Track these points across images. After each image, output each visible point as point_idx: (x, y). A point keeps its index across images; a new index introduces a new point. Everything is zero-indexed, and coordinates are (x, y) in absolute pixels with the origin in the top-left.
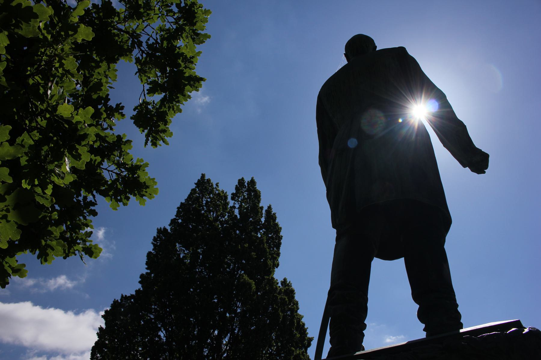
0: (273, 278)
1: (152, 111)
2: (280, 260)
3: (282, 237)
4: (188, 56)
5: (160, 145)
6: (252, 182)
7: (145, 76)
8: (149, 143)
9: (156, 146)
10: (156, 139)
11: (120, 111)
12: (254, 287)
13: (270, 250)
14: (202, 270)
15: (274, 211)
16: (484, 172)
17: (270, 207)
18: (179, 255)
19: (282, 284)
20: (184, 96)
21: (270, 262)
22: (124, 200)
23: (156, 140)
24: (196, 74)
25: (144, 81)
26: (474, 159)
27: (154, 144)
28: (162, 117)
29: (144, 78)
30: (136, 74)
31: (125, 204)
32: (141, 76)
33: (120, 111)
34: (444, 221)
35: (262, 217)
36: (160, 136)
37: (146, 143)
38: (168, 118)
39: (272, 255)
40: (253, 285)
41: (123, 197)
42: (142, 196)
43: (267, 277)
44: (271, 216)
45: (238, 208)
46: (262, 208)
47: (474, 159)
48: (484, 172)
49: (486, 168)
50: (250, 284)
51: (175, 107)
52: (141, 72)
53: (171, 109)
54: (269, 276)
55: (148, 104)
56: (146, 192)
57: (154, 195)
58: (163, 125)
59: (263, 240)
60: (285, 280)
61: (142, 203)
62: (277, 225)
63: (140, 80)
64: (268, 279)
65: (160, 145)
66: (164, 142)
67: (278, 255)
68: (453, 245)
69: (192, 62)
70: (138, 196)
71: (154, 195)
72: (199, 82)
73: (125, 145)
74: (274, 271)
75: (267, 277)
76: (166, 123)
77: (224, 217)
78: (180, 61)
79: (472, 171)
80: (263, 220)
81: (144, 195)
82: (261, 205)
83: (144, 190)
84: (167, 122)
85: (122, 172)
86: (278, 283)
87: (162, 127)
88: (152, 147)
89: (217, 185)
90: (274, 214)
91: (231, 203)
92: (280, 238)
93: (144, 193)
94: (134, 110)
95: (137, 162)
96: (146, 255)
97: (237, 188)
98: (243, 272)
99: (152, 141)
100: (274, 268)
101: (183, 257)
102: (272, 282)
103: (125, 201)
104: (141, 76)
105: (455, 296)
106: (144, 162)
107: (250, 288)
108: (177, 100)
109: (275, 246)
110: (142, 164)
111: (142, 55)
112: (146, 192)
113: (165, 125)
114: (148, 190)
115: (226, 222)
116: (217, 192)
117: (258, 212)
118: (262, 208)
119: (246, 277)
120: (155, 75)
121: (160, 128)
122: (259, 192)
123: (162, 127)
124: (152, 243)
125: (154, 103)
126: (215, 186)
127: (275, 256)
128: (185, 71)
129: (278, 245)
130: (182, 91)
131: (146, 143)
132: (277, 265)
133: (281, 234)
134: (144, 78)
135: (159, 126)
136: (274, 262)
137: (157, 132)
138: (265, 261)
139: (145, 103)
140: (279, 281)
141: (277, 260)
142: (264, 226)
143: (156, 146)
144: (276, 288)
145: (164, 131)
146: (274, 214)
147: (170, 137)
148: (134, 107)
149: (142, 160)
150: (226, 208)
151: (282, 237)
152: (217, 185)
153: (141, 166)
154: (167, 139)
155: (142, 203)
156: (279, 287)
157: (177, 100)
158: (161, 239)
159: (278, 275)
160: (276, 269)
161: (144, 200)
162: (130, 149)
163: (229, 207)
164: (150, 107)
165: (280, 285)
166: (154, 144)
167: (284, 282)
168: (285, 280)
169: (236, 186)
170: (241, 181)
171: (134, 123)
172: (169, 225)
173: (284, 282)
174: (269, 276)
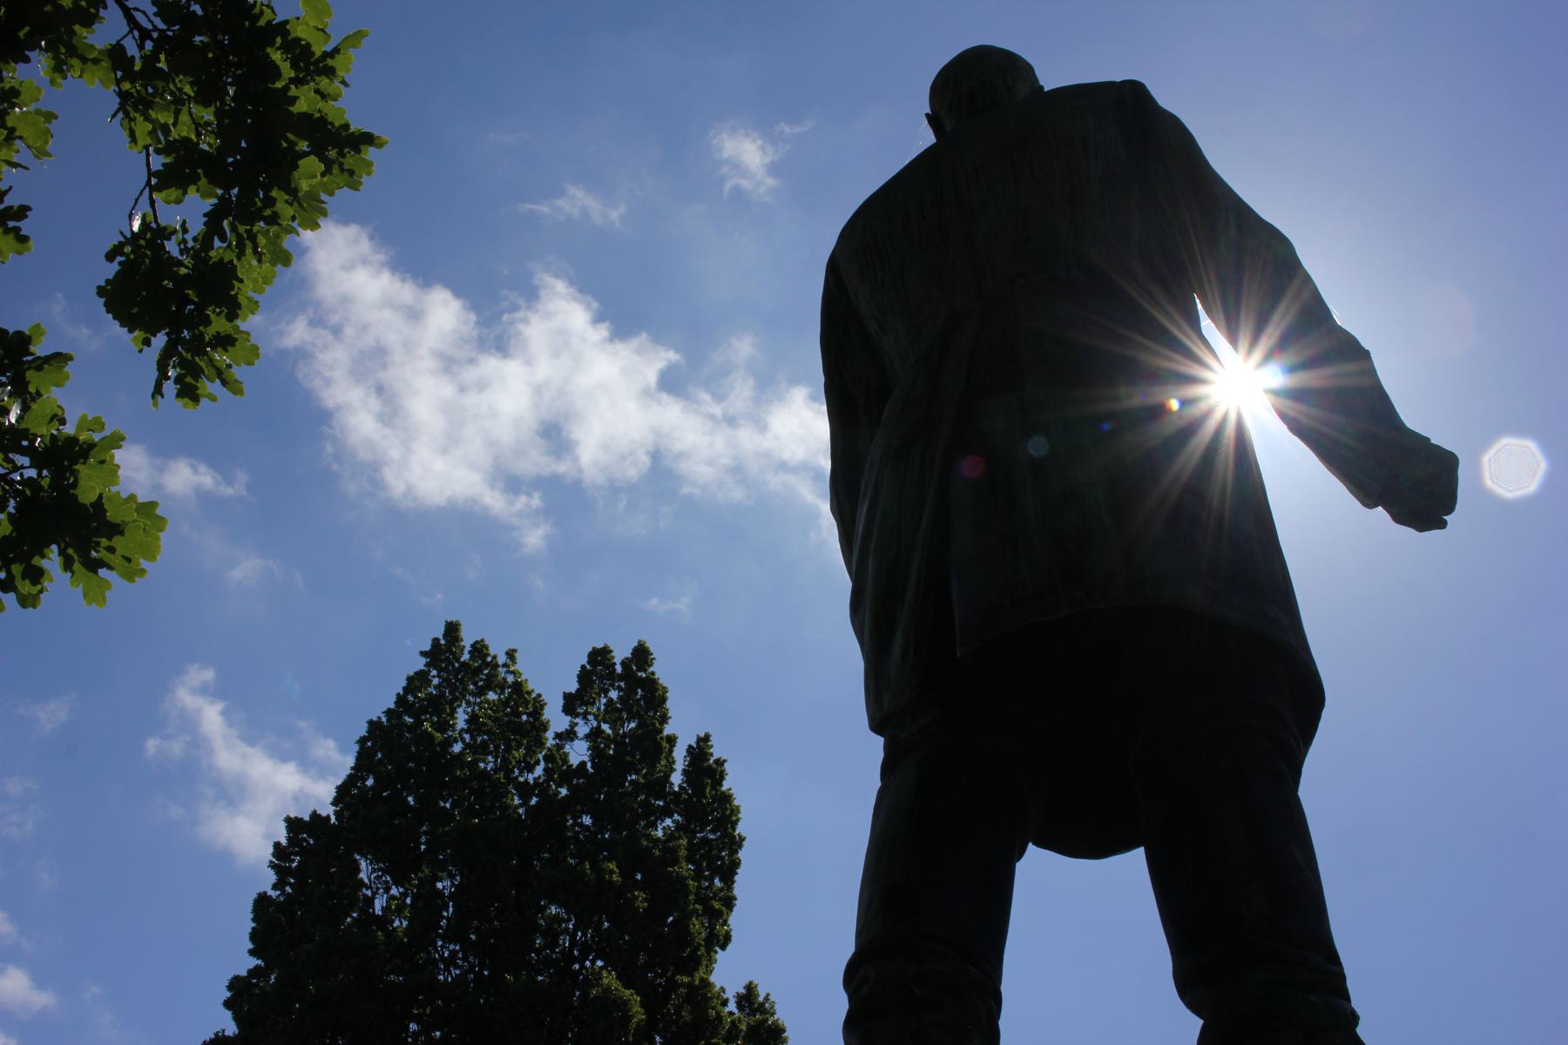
0: (706, 984)
1: (180, 264)
2: (736, 921)
3: (742, 839)
4: (318, 50)
5: (213, 398)
6: (641, 655)
7: (148, 119)
8: (170, 388)
9: (195, 399)
10: (197, 373)
11: (11, 224)
12: (638, 1014)
13: (699, 887)
14: (453, 953)
15: (717, 751)
16: (1442, 525)
17: (704, 740)
18: (370, 902)
19: (740, 1006)
20: (293, 192)
21: (697, 927)
22: (19, 583)
23: (197, 377)
24: (348, 118)
25: (144, 139)
26: (1406, 478)
27: (189, 393)
28: (216, 288)
29: (142, 128)
30: (113, 116)
31: (26, 601)
32: (131, 120)
33: (11, 224)
34: (1301, 698)
35: (672, 770)
36: (211, 361)
37: (158, 391)
38: (245, 291)
39: (703, 900)
40: (637, 1008)
41: (17, 569)
42: (93, 566)
43: (686, 979)
44: (704, 767)
45: (587, 737)
46: (672, 740)
47: (1406, 478)
48: (1442, 525)
49: (1450, 509)
50: (624, 1005)
51: (262, 240)
52: (131, 105)
53: (249, 251)
54: (691, 975)
55: (165, 233)
56: (111, 550)
57: (144, 563)
58: (223, 321)
59: (675, 851)
60: (751, 988)
61: (96, 595)
62: (727, 798)
63: (126, 134)
64: (690, 986)
65: (213, 398)
66: (224, 383)
67: (729, 902)
68: (1328, 786)
69: (330, 72)
70: (77, 566)
71: (144, 563)
72: (358, 151)
73: (39, 368)
74: (711, 961)
75: (686, 979)
76: (233, 310)
77: (531, 769)
78: (277, 56)
79: (1398, 519)
80: (677, 779)
81: (101, 564)
82: (668, 730)
83: (104, 542)
84: (239, 306)
85: (16, 469)
86: (725, 1003)
87: (219, 325)
88: (180, 403)
89: (511, 654)
90: (720, 762)
91: (556, 720)
92: (736, 844)
93: (103, 554)
94: (110, 257)
95: (80, 428)
96: (249, 906)
97: (584, 676)
98: (600, 963)
99: (178, 380)
100: (710, 949)
101: (385, 909)
102: (702, 995)
103: (26, 587)
104: (131, 120)
105: (1343, 978)
106: (107, 432)
107: (626, 1018)
108: (268, 212)
109: (715, 872)
110: (96, 437)
111: (141, 47)
112: (111, 550)
113: (232, 316)
114: (117, 541)
115: (540, 787)
116: (510, 679)
117: (659, 749)
118: (672, 740)
119: (610, 979)
120: (194, 122)
121: (209, 332)
122: (665, 690)
123: (219, 325)
124: (272, 866)
125: (185, 231)
126: (502, 659)
127: (717, 905)
128: (293, 91)
129: (729, 871)
130: (280, 170)
131: (158, 391)
132: (725, 941)
133: (741, 829)
134: (142, 128)
135: (208, 322)
136: (712, 927)
137: (198, 346)
138: (684, 918)
139: (155, 234)
140: (730, 994)
141: (725, 923)
142: (675, 802)
143: (195, 399)
144: (719, 1018)
145: (226, 342)
146: (720, 762)
147: (250, 363)
148: (109, 247)
149: (98, 424)
150: (540, 743)
151: (742, 839)
152: (511, 654)
153: (92, 446)
154: (238, 372)
155: (96, 595)
156: (731, 1013)
157: (268, 212)
158: (304, 852)
159: (728, 974)
160: (720, 955)
161: (106, 585)
162: (58, 385)
163: (550, 735)
164: (172, 247)
165: (732, 1006)
166: (189, 393)
167: (748, 999)
168: (751, 988)
169: (583, 667)
170: (600, 656)
171: (106, 304)
172: (334, 803)
173: (748, 999)
174: (691, 975)
